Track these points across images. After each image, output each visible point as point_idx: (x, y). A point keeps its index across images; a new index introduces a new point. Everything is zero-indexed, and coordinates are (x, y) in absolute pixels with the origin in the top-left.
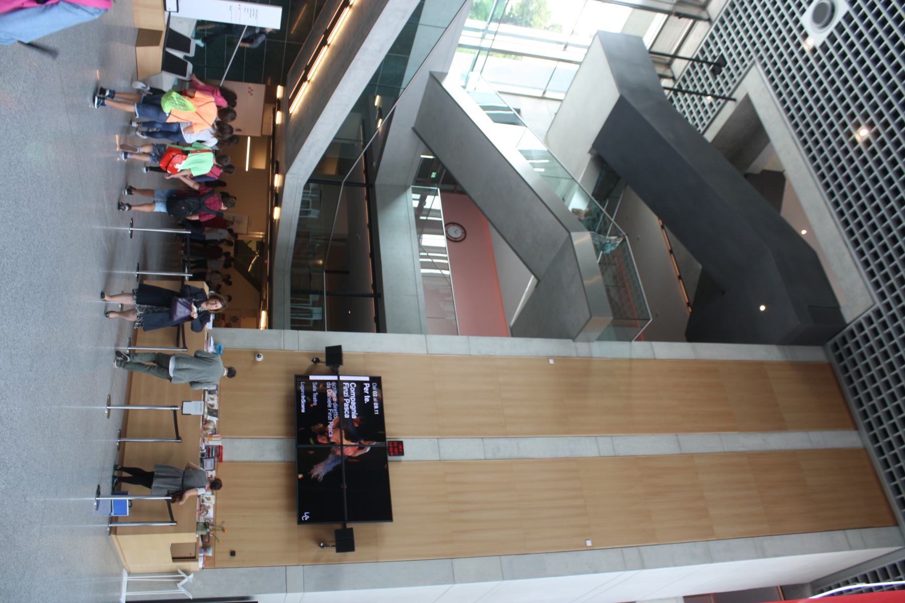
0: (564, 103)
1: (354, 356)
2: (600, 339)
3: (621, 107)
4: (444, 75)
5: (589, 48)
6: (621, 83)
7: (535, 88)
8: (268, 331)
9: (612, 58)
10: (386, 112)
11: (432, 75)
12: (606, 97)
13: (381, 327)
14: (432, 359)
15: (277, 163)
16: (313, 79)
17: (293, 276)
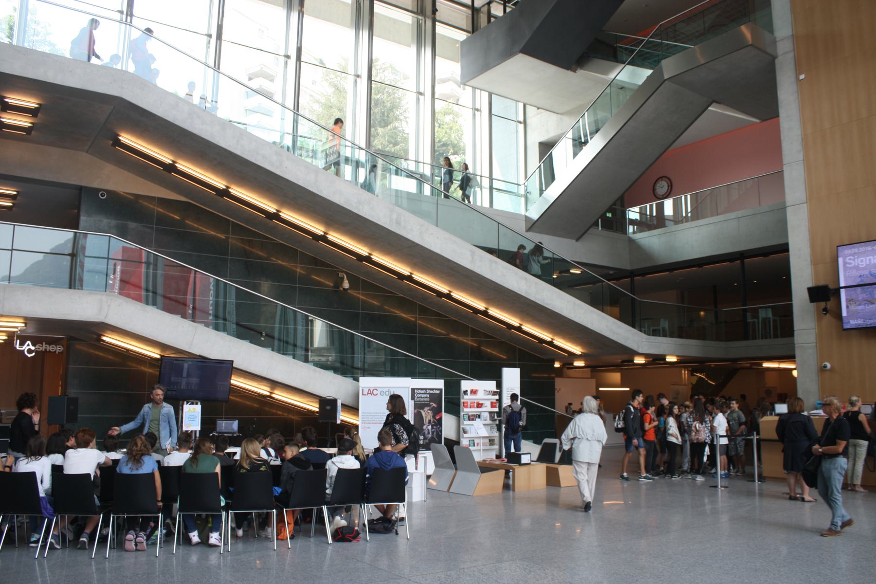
0: (525, 102)
1: (816, 273)
2: (771, 30)
3: (531, 50)
4: (527, 219)
5: (474, 88)
6: (508, 54)
7: (517, 131)
8: (797, 359)
9: (486, 67)
10: (562, 265)
11: (529, 230)
12: (523, 68)
13: (784, 248)
14: (813, 197)
15: (623, 361)
16: (551, 336)
17: (729, 339)
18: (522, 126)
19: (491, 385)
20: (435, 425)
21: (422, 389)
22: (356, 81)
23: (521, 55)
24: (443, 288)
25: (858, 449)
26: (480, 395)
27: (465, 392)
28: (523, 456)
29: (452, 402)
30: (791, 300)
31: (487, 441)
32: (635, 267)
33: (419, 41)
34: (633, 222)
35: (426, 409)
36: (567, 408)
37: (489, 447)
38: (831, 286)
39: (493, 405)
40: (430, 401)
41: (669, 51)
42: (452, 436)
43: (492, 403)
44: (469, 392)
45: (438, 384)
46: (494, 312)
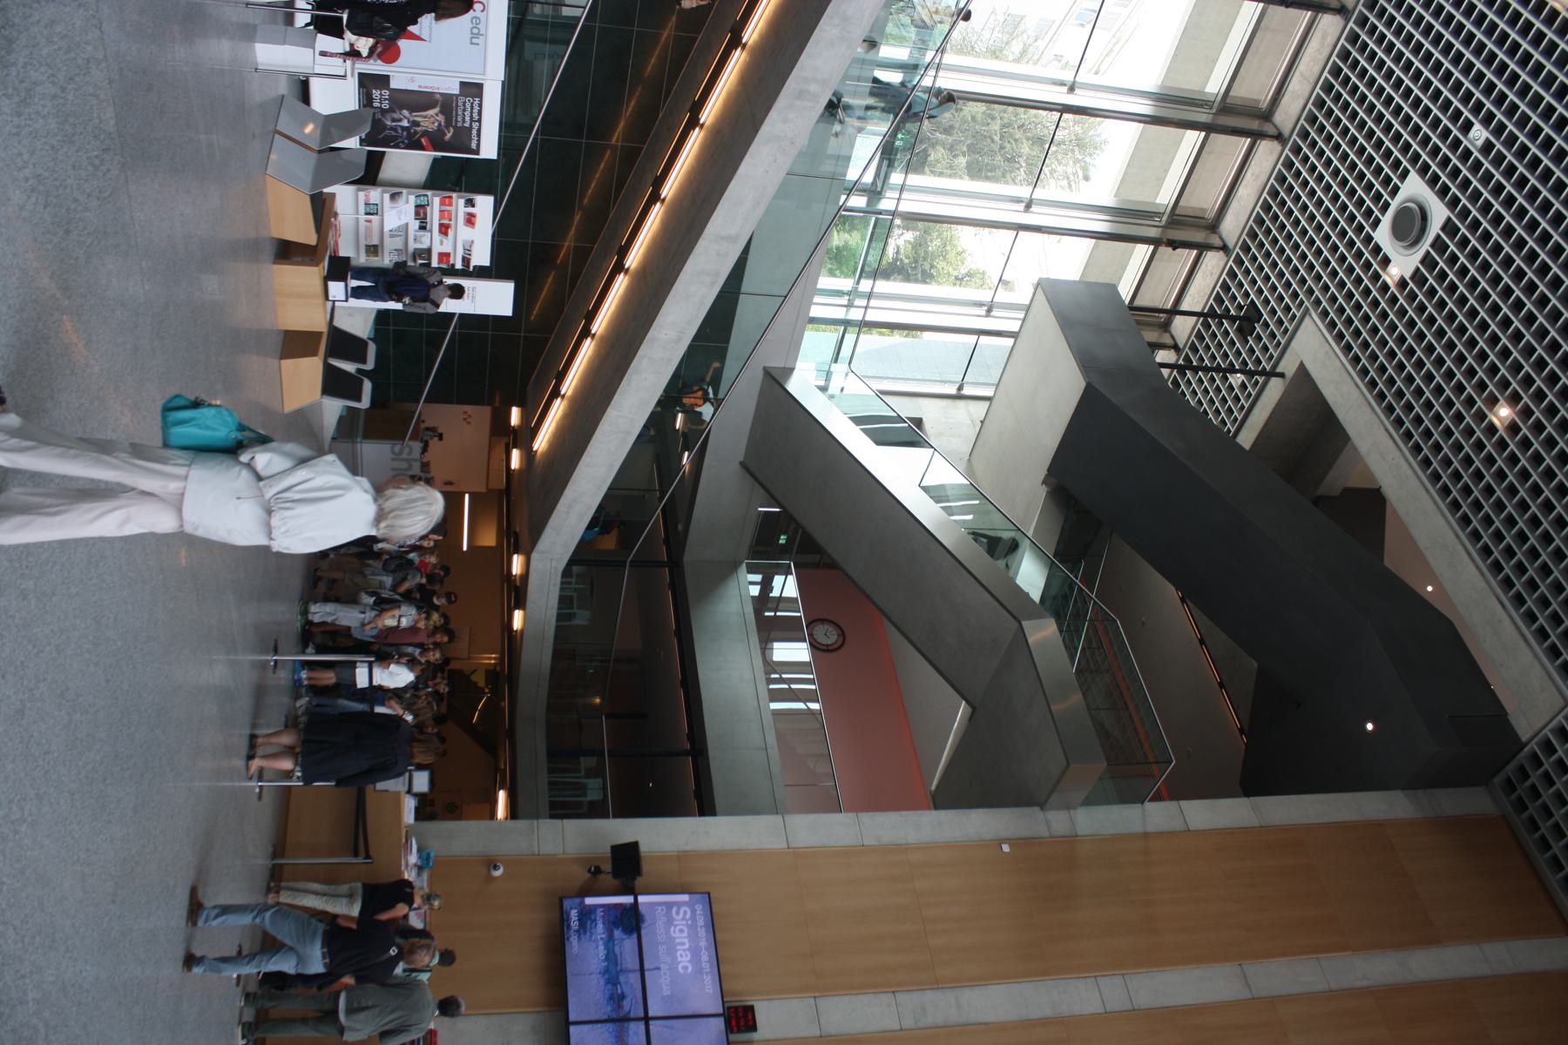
1: (663, 858)
2: (1089, 802)
5: (1028, 309)
6: (1086, 362)
8: (511, 823)
9: (1067, 323)
13: (705, 806)
14: (798, 858)
15: (516, 535)
16: (569, 393)
18: (953, 391)
19: (482, 257)
20: (410, 136)
21: (480, 113)
22: (1062, 84)
23: (1083, 384)
24: (669, 189)
25: (345, 901)
26: (463, 233)
27: (470, 203)
28: (342, 284)
29: (455, 175)
30: (615, 816)
31: (375, 241)
32: (688, 572)
33: (1119, 213)
34: (766, 585)
35: (441, 118)
36: (433, 429)
37: (363, 243)
38: (639, 882)
39: (444, 256)
40: (456, 128)
41: (1069, 634)
42: (388, 171)
43: (448, 255)
44: (470, 210)
45: (489, 149)
46: (621, 284)
